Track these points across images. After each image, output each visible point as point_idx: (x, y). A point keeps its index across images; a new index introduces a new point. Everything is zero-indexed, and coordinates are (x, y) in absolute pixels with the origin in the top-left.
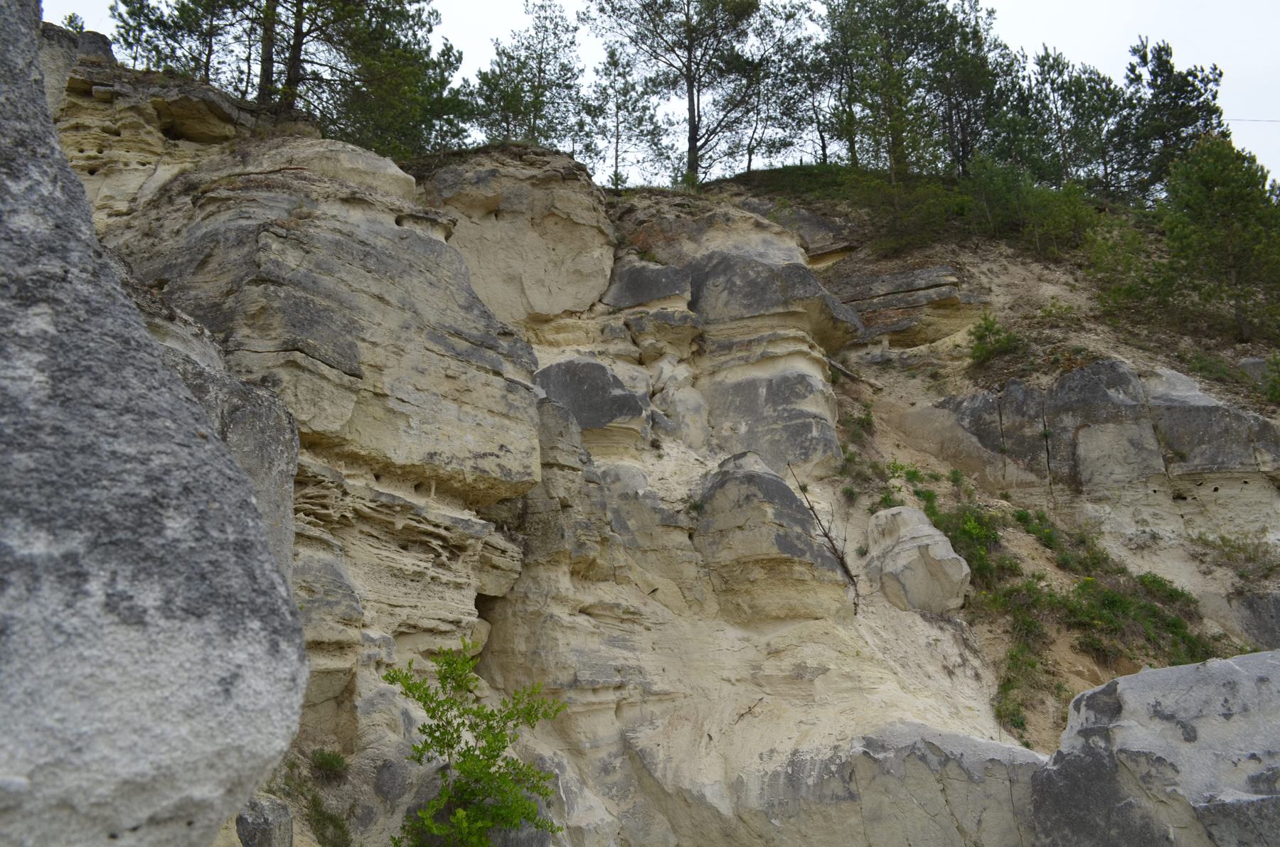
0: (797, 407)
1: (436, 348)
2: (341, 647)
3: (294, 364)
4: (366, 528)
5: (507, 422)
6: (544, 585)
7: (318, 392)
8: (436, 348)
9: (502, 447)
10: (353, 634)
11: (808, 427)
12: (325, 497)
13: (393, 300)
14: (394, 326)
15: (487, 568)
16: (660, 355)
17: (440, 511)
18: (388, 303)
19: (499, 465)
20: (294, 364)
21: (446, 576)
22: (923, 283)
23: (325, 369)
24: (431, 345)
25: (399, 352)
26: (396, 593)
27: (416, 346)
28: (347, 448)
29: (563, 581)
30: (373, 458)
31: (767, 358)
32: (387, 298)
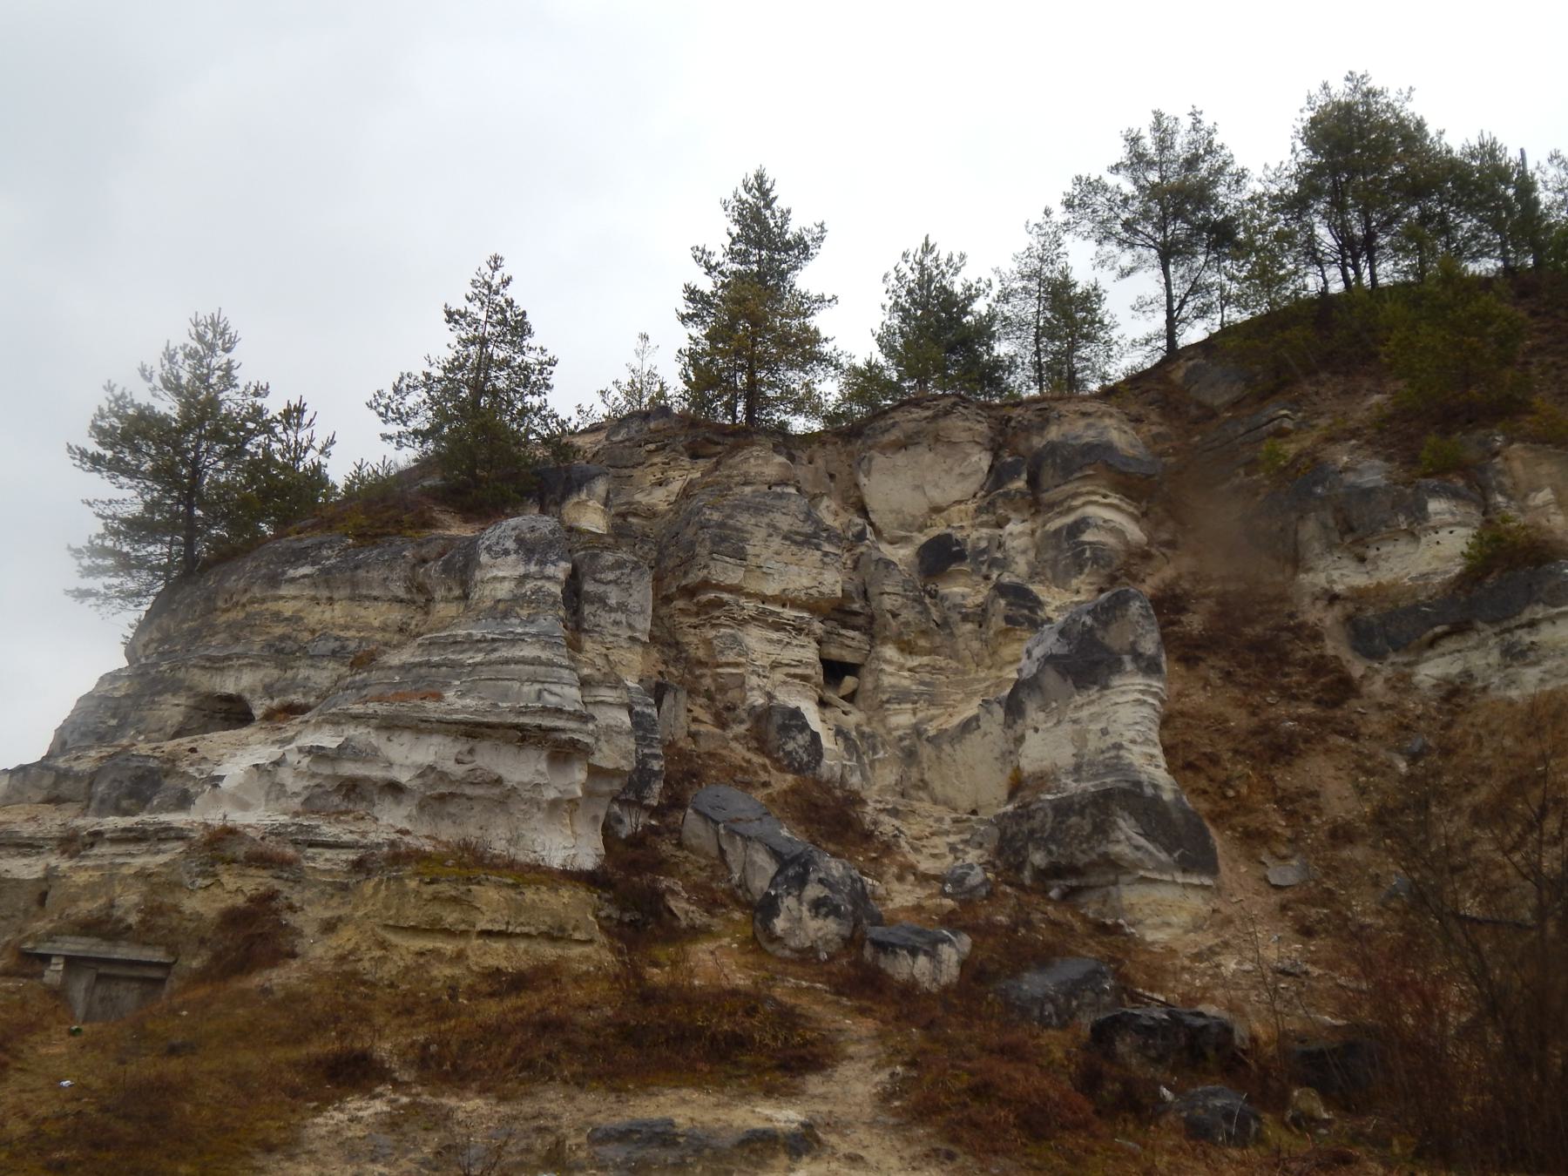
2: (737, 665)
10: (743, 660)
11: (1083, 551)
16: (1008, 520)
17: (789, 613)
21: (795, 642)
22: (1265, 420)
26: (770, 648)
27: (776, 543)
29: (890, 651)
31: (1071, 509)
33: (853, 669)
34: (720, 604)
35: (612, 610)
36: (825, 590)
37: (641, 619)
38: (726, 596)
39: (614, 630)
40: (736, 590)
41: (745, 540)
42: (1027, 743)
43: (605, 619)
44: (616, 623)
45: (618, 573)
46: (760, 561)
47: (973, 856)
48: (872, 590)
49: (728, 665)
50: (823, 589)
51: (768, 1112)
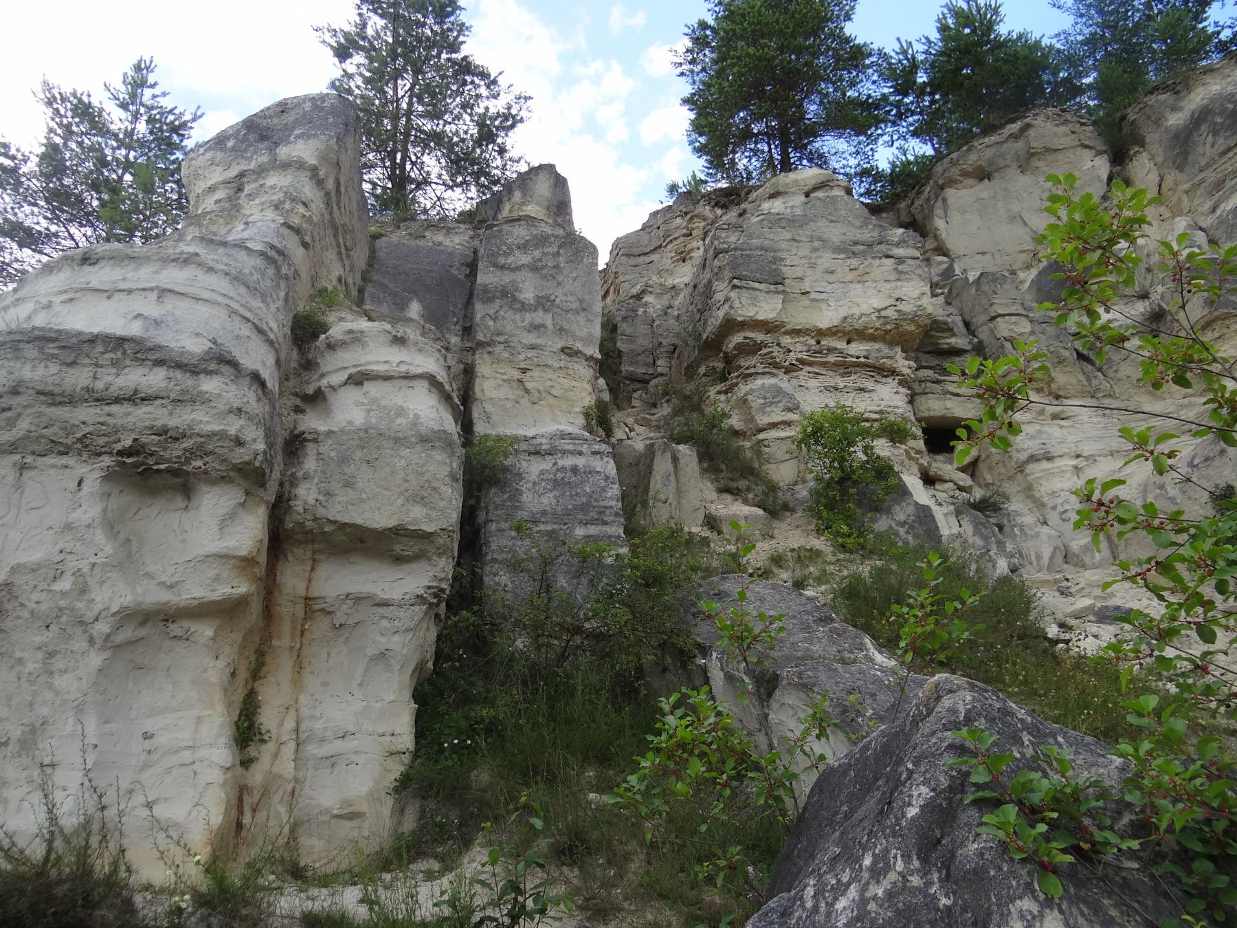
3: (735, 287)
4: (810, 369)
5: (900, 283)
7: (755, 298)
13: (803, 239)
15: (948, 396)
17: (858, 349)
18: (800, 241)
20: (735, 287)
23: (756, 285)
25: (813, 266)
27: (826, 260)
28: (789, 327)
34: (751, 348)
35: (524, 307)
36: (906, 307)
37: (581, 319)
38: (759, 337)
39: (531, 339)
40: (769, 327)
41: (775, 260)
43: (513, 323)
44: (536, 328)
45: (537, 253)
46: (806, 286)
47: (736, 741)
49: (774, 425)
50: (904, 307)
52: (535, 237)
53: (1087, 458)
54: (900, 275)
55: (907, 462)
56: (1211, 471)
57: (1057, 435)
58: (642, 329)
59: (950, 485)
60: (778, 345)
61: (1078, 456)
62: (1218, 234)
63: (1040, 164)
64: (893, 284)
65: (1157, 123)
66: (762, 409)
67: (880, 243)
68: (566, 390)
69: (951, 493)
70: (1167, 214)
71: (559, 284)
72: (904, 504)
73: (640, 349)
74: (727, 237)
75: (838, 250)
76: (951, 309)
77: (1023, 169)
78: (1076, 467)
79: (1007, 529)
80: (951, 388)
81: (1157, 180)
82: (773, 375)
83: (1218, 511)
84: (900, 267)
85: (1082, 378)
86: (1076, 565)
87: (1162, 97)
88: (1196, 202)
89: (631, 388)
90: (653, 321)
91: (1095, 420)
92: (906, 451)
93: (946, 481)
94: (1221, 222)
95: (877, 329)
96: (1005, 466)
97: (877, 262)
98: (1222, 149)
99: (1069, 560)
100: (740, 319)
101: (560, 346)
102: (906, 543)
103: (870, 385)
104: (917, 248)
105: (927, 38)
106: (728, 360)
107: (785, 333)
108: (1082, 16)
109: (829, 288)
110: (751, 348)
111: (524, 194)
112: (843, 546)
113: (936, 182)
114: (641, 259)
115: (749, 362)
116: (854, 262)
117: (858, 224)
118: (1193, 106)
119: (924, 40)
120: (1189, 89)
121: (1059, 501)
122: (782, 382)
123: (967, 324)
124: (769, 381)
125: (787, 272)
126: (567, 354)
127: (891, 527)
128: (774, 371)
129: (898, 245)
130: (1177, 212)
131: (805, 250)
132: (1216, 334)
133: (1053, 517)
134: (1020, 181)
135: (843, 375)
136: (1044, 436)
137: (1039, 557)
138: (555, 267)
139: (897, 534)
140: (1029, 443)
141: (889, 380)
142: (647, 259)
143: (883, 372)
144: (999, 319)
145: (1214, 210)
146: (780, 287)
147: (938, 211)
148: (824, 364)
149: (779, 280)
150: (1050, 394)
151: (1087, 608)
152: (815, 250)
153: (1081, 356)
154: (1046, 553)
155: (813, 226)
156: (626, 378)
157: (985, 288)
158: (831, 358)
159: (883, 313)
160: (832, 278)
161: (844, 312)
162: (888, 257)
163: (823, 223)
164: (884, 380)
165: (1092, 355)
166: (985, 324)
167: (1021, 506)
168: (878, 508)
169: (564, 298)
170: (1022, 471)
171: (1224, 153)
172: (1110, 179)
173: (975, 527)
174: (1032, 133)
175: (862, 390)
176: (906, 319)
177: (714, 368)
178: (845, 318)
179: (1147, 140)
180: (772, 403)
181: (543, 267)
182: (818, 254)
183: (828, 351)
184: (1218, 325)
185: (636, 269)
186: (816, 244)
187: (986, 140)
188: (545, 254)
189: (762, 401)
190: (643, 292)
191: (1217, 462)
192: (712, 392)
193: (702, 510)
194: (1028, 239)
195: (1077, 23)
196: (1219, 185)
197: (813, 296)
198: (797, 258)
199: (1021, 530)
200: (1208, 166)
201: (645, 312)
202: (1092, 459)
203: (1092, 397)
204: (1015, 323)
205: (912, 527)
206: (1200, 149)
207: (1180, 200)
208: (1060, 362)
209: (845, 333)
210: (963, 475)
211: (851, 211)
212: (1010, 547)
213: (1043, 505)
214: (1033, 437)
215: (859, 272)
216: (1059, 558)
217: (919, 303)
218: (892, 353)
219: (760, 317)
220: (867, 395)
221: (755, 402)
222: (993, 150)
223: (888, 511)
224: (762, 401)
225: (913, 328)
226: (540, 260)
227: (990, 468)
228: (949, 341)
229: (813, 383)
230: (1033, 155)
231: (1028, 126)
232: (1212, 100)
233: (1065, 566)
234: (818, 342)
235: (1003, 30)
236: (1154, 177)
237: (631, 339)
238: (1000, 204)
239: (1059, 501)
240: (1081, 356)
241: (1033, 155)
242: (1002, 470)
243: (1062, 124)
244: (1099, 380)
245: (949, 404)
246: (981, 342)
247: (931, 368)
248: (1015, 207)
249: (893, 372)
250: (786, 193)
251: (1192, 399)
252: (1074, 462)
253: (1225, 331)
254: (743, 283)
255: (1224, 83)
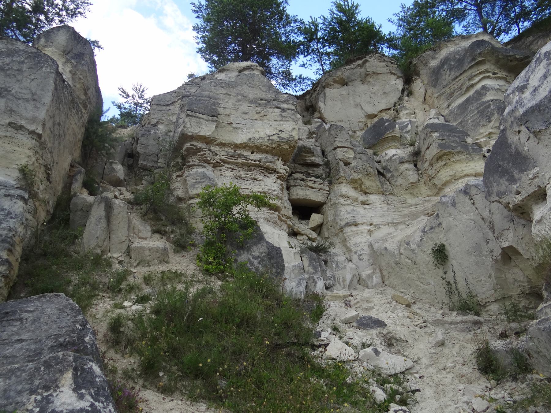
0: (483, 100)
1: (252, 106)
3: (188, 115)
4: (228, 166)
5: (282, 122)
6: (337, 192)
8: (252, 106)
9: (280, 131)
12: (205, 154)
13: (233, 94)
14: (234, 101)
17: (256, 157)
18: (231, 95)
19: (278, 137)
20: (188, 115)
23: (201, 116)
24: (250, 105)
27: (244, 106)
28: (218, 141)
29: (345, 189)
30: (229, 144)
32: (230, 93)
33: (317, 207)
34: (195, 151)
36: (284, 135)
37: (30, 106)
38: (199, 145)
40: (208, 141)
41: (215, 104)
42: (436, 183)
45: (7, 60)
46: (231, 120)
48: (329, 149)
50: (283, 135)
51: (239, 152)
52: (9, 50)
53: (375, 226)
54: (283, 118)
55: (279, 222)
56: (433, 235)
57: (362, 213)
58: (152, 142)
59: (305, 237)
60: (210, 150)
61: (371, 225)
62: (449, 118)
63: (370, 80)
64: (278, 123)
65: (426, 65)
66: (193, 186)
67: (274, 100)
68: (7, 152)
69: (305, 242)
70: (428, 108)
71: (18, 81)
72: (260, 245)
73: (150, 153)
74: (191, 89)
75: (251, 102)
76: (317, 144)
77: (363, 82)
78: (369, 231)
79: (329, 263)
80: (310, 184)
81: (424, 92)
82: (204, 167)
83: (436, 259)
84: (283, 114)
85: (379, 184)
86: (364, 286)
87: (428, 53)
88: (441, 102)
89: (143, 174)
90: (159, 138)
91: (383, 206)
92: (278, 216)
93: (303, 235)
94: (451, 112)
95: (267, 146)
96: (334, 228)
97: (272, 110)
98: (453, 77)
99: (361, 282)
100: (189, 134)
101: (8, 121)
102: (257, 269)
103: (260, 177)
104: (294, 105)
105: (323, 16)
106: (184, 158)
107: (217, 145)
108: (401, 26)
109: (244, 122)
110: (195, 151)
111: (47, 41)
112: (207, 270)
113: (322, 85)
114: (164, 108)
115: (194, 160)
116: (259, 109)
117: (265, 90)
118: (441, 57)
119: (322, 17)
120: (440, 48)
121: (359, 249)
122: (208, 171)
123: (323, 152)
124: (200, 170)
125: (221, 111)
126: (13, 128)
127: (249, 259)
128: (206, 165)
129: (284, 102)
130: (431, 107)
131: (233, 100)
132: (444, 163)
133: (355, 258)
134: (362, 88)
135: (246, 171)
136: (355, 213)
137: (344, 280)
138: (18, 70)
139: (252, 264)
140: (347, 216)
141: (272, 175)
142: (168, 108)
143: (269, 170)
144: (338, 149)
145: (448, 107)
146: (215, 118)
147: (321, 99)
148: (236, 164)
149: (215, 114)
150: (361, 191)
151: (353, 317)
152: (239, 101)
153: (379, 173)
154: (349, 278)
155: (239, 88)
156: (141, 168)
157: (333, 132)
158: (240, 161)
159: (271, 138)
160: (246, 116)
161: (250, 136)
162: (278, 108)
163: (245, 87)
164: (269, 175)
165: (384, 172)
166: (331, 151)
167: (339, 250)
168: (242, 247)
169: (19, 91)
170: (342, 231)
171: (454, 79)
172: (403, 91)
173: (310, 261)
174: (368, 64)
175: (255, 179)
176: (283, 142)
177: (178, 162)
178: (251, 139)
179: (421, 73)
180: (199, 182)
181: (9, 69)
182: (240, 103)
183: (241, 157)
184: (445, 158)
185: (161, 113)
186: (240, 98)
187: (347, 67)
188: (13, 61)
189: (194, 181)
190: (158, 122)
191: (437, 230)
192: (174, 176)
193: (127, 242)
194: (363, 116)
195: (398, 29)
196: (451, 95)
197: (234, 125)
198: (227, 104)
199: (337, 264)
200: (447, 85)
201: (155, 133)
202: (378, 226)
203: (383, 194)
204: (346, 152)
205: (262, 260)
206: (444, 77)
207: (433, 101)
208: (368, 174)
209: (250, 148)
210: (313, 233)
211: (262, 82)
212: (329, 273)
213: (351, 251)
214: (349, 213)
215: (261, 114)
216: (355, 281)
217: (291, 134)
218: (273, 160)
219: (202, 134)
220: (258, 182)
221: (190, 181)
222: (350, 72)
223: (249, 250)
224: (194, 181)
225: (287, 147)
226: (8, 64)
227: (328, 229)
228: (311, 158)
229: (228, 174)
230: (367, 75)
231: (367, 61)
232: (450, 54)
233: (358, 286)
234: (235, 151)
235: (359, 17)
236: (422, 91)
237: (145, 146)
238: (351, 98)
239: (359, 249)
240: (379, 173)
241: (367, 75)
242: (333, 230)
243: (382, 61)
244: (387, 185)
245: (308, 192)
246: (328, 161)
247: (302, 173)
248: (358, 100)
249: (274, 171)
250: (228, 70)
251: (431, 197)
252: (369, 228)
253: (448, 161)
254: (193, 114)
255: (456, 47)
